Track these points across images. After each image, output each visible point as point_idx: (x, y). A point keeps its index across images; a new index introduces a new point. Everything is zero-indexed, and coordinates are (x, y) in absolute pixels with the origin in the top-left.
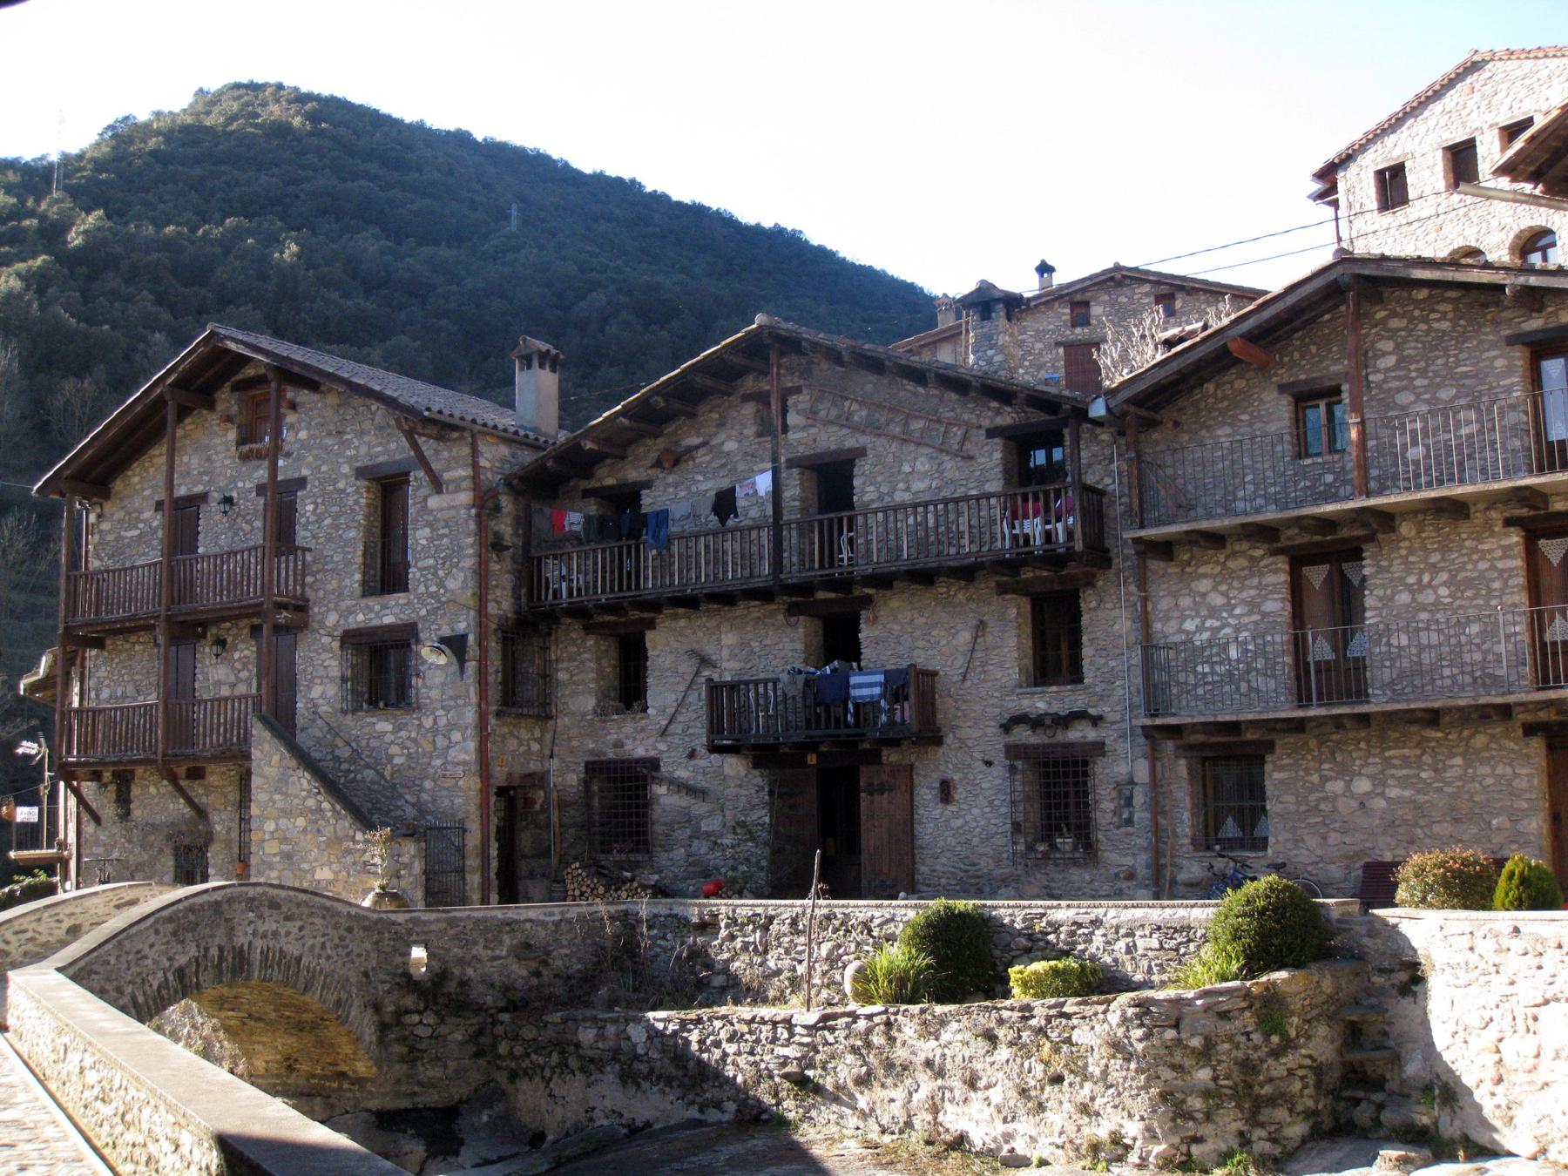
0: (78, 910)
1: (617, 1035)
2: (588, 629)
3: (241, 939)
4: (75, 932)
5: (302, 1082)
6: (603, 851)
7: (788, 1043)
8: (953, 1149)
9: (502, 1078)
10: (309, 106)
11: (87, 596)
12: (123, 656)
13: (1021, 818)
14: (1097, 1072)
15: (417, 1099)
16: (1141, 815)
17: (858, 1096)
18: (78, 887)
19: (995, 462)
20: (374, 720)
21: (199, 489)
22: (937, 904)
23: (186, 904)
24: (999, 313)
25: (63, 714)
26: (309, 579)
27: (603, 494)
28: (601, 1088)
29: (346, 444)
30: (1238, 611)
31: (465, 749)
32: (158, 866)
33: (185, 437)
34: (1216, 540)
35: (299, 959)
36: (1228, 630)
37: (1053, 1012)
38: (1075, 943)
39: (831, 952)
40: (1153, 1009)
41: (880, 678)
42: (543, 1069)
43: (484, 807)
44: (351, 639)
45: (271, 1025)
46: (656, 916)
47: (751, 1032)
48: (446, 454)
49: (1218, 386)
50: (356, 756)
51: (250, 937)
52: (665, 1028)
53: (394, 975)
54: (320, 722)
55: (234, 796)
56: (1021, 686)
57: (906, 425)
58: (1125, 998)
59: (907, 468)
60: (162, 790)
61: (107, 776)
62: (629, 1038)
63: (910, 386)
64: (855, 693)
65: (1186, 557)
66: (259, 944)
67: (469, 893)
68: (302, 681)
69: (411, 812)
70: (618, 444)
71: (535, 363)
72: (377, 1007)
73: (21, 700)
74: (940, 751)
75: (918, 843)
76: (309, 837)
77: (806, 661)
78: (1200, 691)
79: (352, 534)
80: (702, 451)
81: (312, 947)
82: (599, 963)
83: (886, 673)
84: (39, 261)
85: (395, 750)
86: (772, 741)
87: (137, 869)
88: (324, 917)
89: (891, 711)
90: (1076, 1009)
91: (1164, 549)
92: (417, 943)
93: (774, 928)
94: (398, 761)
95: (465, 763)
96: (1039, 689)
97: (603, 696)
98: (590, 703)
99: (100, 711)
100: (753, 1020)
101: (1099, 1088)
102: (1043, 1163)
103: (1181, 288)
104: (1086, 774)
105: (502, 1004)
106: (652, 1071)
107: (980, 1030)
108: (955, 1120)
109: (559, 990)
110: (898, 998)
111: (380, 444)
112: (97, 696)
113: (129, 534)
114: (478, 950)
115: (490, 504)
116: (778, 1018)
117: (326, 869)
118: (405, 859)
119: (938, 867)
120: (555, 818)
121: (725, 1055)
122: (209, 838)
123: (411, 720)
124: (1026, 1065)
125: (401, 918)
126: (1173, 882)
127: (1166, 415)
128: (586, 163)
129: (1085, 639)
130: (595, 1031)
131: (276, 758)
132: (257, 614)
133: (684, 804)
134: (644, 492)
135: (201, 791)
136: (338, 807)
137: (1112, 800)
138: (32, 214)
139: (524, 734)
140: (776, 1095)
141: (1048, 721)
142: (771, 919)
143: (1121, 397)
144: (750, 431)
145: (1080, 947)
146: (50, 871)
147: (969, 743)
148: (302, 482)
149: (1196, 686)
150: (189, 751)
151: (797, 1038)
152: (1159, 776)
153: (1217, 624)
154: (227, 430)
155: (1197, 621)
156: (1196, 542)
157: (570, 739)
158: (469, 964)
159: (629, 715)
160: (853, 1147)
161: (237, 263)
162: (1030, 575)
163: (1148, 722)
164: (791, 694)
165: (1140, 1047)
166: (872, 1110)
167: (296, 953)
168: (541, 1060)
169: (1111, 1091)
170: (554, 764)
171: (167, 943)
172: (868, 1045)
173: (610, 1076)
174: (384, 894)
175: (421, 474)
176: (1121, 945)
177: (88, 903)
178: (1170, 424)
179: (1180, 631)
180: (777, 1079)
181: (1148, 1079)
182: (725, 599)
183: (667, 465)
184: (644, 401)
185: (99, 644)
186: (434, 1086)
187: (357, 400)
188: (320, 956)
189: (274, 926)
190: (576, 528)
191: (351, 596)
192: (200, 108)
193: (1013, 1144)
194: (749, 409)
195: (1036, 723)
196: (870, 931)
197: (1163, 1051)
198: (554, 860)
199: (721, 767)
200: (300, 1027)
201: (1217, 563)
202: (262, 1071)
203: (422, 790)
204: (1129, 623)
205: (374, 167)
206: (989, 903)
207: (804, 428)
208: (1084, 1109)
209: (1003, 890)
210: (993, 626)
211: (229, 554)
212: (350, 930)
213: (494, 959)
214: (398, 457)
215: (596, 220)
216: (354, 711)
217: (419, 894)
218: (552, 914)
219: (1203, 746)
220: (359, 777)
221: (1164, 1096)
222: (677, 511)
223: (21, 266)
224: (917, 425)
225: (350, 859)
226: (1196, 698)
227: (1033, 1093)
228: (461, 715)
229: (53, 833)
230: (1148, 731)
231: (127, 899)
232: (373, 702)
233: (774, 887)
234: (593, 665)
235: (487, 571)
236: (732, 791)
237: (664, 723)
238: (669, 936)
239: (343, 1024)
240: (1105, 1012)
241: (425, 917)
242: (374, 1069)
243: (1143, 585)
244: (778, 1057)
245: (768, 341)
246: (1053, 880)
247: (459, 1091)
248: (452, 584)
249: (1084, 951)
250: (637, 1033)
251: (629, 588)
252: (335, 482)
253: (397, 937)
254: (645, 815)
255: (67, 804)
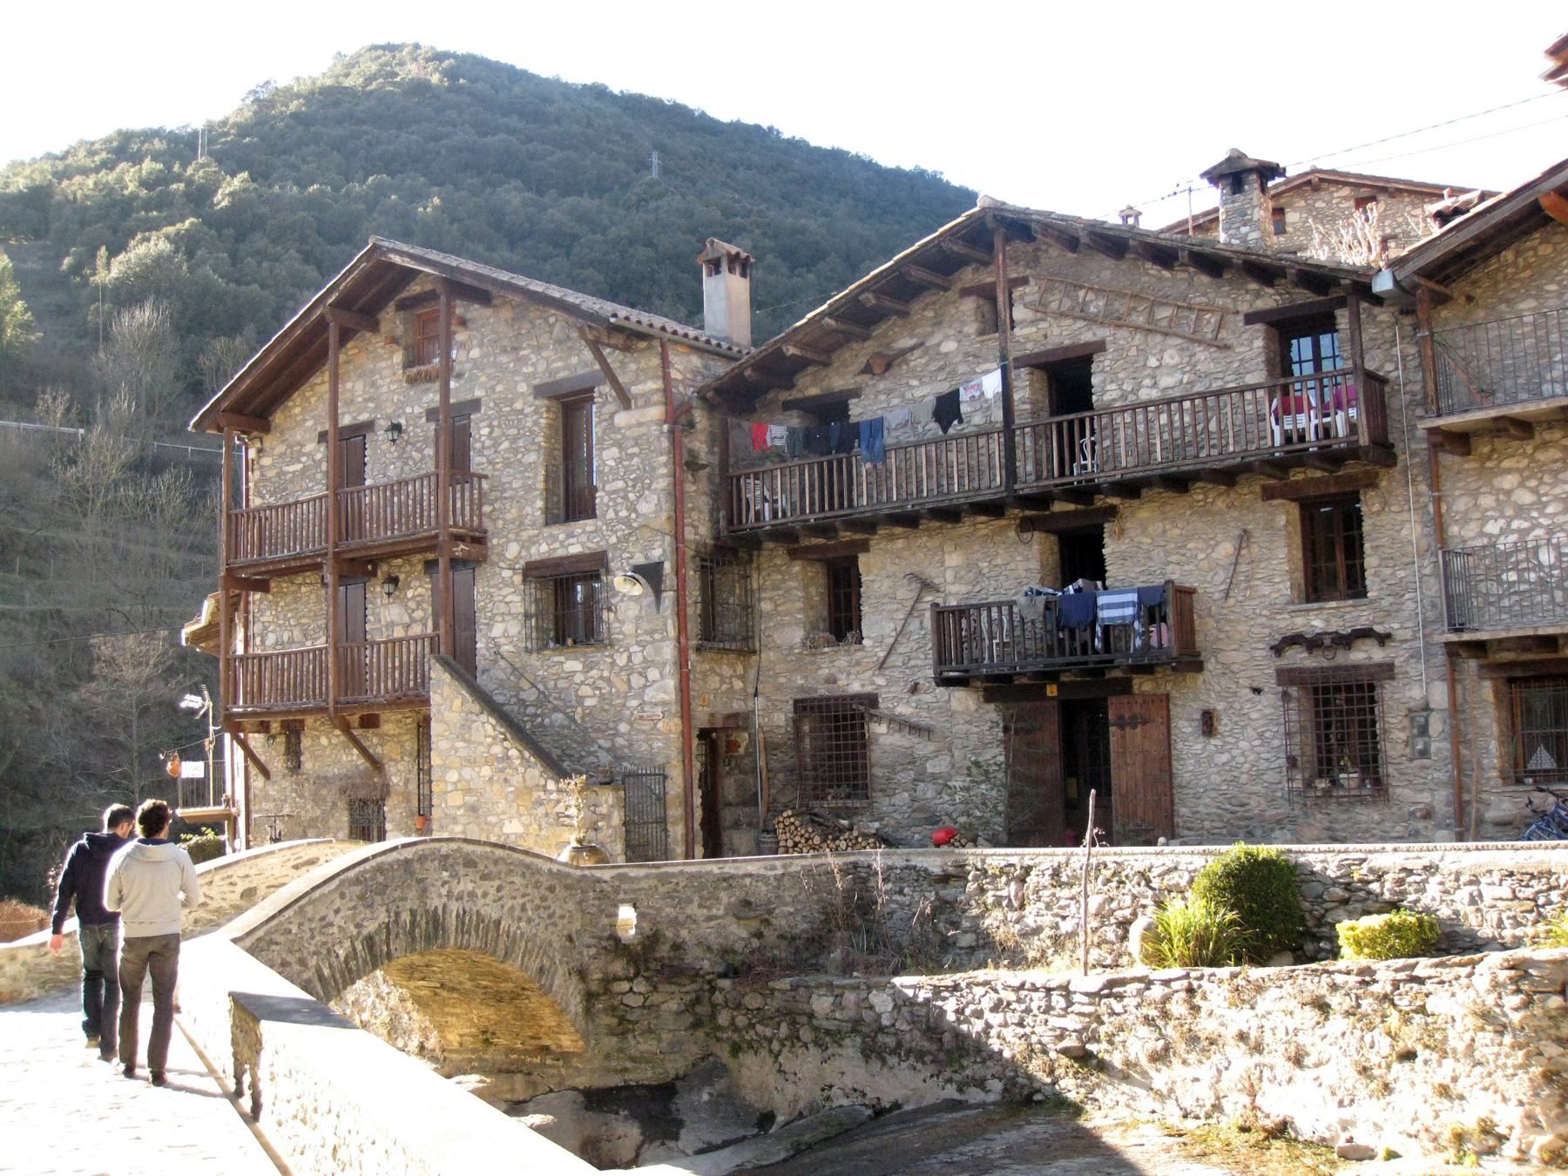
0: (253, 872)
1: (857, 1005)
2: (794, 555)
3: (435, 902)
4: (249, 895)
5: (500, 1058)
6: (817, 798)
7: (1066, 1012)
8: (1275, 1137)
9: (723, 1052)
10: (446, 64)
11: (250, 535)
12: (289, 599)
13: (1296, 752)
14: (1461, 1047)
15: (627, 1076)
16: (1439, 745)
17: (1152, 1073)
18: (248, 847)
19: (1257, 351)
20: (562, 658)
21: (364, 417)
22: (1236, 851)
23: (373, 863)
24: (1253, 181)
25: (228, 661)
26: (486, 509)
27: (806, 406)
28: (839, 1063)
29: (522, 361)
30: (1550, 509)
31: (664, 688)
32: (332, 822)
33: (347, 362)
34: (1523, 428)
35: (498, 923)
36: (1539, 532)
37: (1402, 976)
38: (1404, 893)
39: (1101, 906)
40: (1532, 971)
41: (1133, 597)
42: (770, 1041)
43: (686, 750)
44: (534, 572)
45: (466, 995)
46: (890, 868)
47: (1019, 1001)
48: (633, 366)
49: (1518, 254)
50: (543, 698)
51: (445, 900)
52: (916, 996)
53: (601, 938)
54: (502, 663)
55: (410, 745)
56: (1292, 602)
57: (1151, 314)
58: (1494, 959)
59: (1153, 362)
60: (334, 741)
61: (275, 727)
62: (871, 1007)
63: (1153, 270)
64: (1104, 614)
65: (1486, 450)
66: (454, 907)
67: (672, 846)
68: (481, 619)
69: (605, 758)
70: (823, 348)
71: (724, 267)
72: (582, 974)
73: (183, 655)
74: (1201, 677)
75: (1177, 781)
76: (496, 787)
77: (1042, 582)
78: (1506, 602)
79: (532, 457)
80: (917, 353)
81: (512, 908)
82: (827, 921)
83: (1140, 591)
84: (187, 223)
85: (585, 690)
86: (1006, 670)
87: (309, 826)
88: (523, 875)
89: (1146, 633)
90: (1432, 972)
91: (1460, 441)
92: (623, 901)
93: (1032, 880)
94: (589, 702)
95: (664, 703)
96: (1316, 605)
97: (813, 627)
98: (797, 635)
99: (266, 657)
100: (1022, 986)
101: (1463, 1067)
102: (1392, 1155)
103: (1384, 190)
104: (1372, 700)
105: (720, 969)
106: (899, 1044)
107: (1307, 997)
108: (1276, 1104)
109: (782, 952)
110: (1197, 961)
111: (560, 359)
112: (263, 642)
113: (291, 468)
114: (693, 909)
115: (683, 420)
116: (1053, 985)
117: (515, 822)
118: (603, 810)
119: (1201, 809)
120: (761, 763)
121: (988, 1026)
122: (386, 791)
123: (601, 657)
124: (1368, 1039)
125: (607, 875)
126: (1480, 821)
127: (1458, 289)
128: (723, 112)
129: (1367, 546)
130: (831, 999)
131: (458, 702)
132: (432, 548)
133: (906, 743)
134: (852, 401)
135: (375, 740)
136: (527, 754)
137: (1403, 729)
138: (178, 178)
139: (727, 671)
140: (1051, 1072)
141: (1327, 641)
142: (1027, 870)
143: (1412, 267)
144: (971, 328)
145: (1411, 898)
146: (218, 829)
147: (1235, 668)
148: (475, 404)
149: (1500, 598)
150: (362, 698)
151: (1076, 1008)
152: (1460, 700)
153: (1525, 525)
154: (393, 353)
155: (1502, 522)
156: (1505, 430)
157: (777, 675)
158: (682, 925)
159: (843, 647)
160: (1153, 1136)
161: (382, 219)
162: (1300, 477)
163: (1454, 638)
164: (1029, 618)
165: (1516, 1017)
166: (1171, 1091)
167: (495, 916)
168: (768, 1032)
169: (1479, 1069)
170: (760, 702)
171: (354, 908)
172: (1165, 1015)
173: (851, 1048)
174: (583, 847)
175: (606, 388)
176: (1463, 894)
177: (262, 863)
178: (1462, 300)
179: (1482, 534)
180: (1053, 1055)
181: (1528, 1056)
182: (949, 515)
183: (877, 371)
184: (853, 299)
185: (263, 587)
186: (648, 1062)
187: (534, 312)
188: (520, 919)
189: (470, 887)
190: (778, 443)
191: (533, 525)
192: (339, 69)
193: (1352, 1132)
194: (969, 304)
195: (1313, 643)
196: (1148, 882)
197: (1546, 1023)
198: (762, 808)
199: (949, 701)
200: (499, 998)
201: (1524, 455)
202: (456, 1045)
203: (617, 734)
204: (1419, 528)
205: (513, 121)
206: (1295, 847)
207: (1033, 322)
208: (1444, 1091)
209: (1277, 833)
210: (1258, 534)
211: (399, 483)
212: (551, 889)
213: (710, 918)
214: (580, 372)
215: (735, 168)
216: (540, 650)
217: (619, 847)
218: (773, 868)
219: (1512, 665)
220: (547, 721)
221: (1549, 1077)
222: (893, 419)
223: (170, 230)
224: (1163, 313)
225: (541, 810)
226: (1501, 610)
227: (1376, 1072)
228: (658, 651)
229: (220, 790)
230: (1453, 650)
231: (306, 858)
232: (560, 640)
233: (1010, 834)
234: (800, 594)
235: (682, 491)
236: (961, 728)
237: (882, 654)
238: (906, 890)
239: (546, 994)
240: (1470, 976)
241: (633, 873)
242: (581, 1043)
243: (1435, 484)
244: (1053, 1029)
245: (991, 224)
246: (1335, 821)
247: (675, 1066)
248: (645, 507)
249: (1417, 901)
250: (881, 1002)
251: (841, 506)
252: (512, 402)
253: (602, 895)
254: (864, 757)
255: (234, 756)
